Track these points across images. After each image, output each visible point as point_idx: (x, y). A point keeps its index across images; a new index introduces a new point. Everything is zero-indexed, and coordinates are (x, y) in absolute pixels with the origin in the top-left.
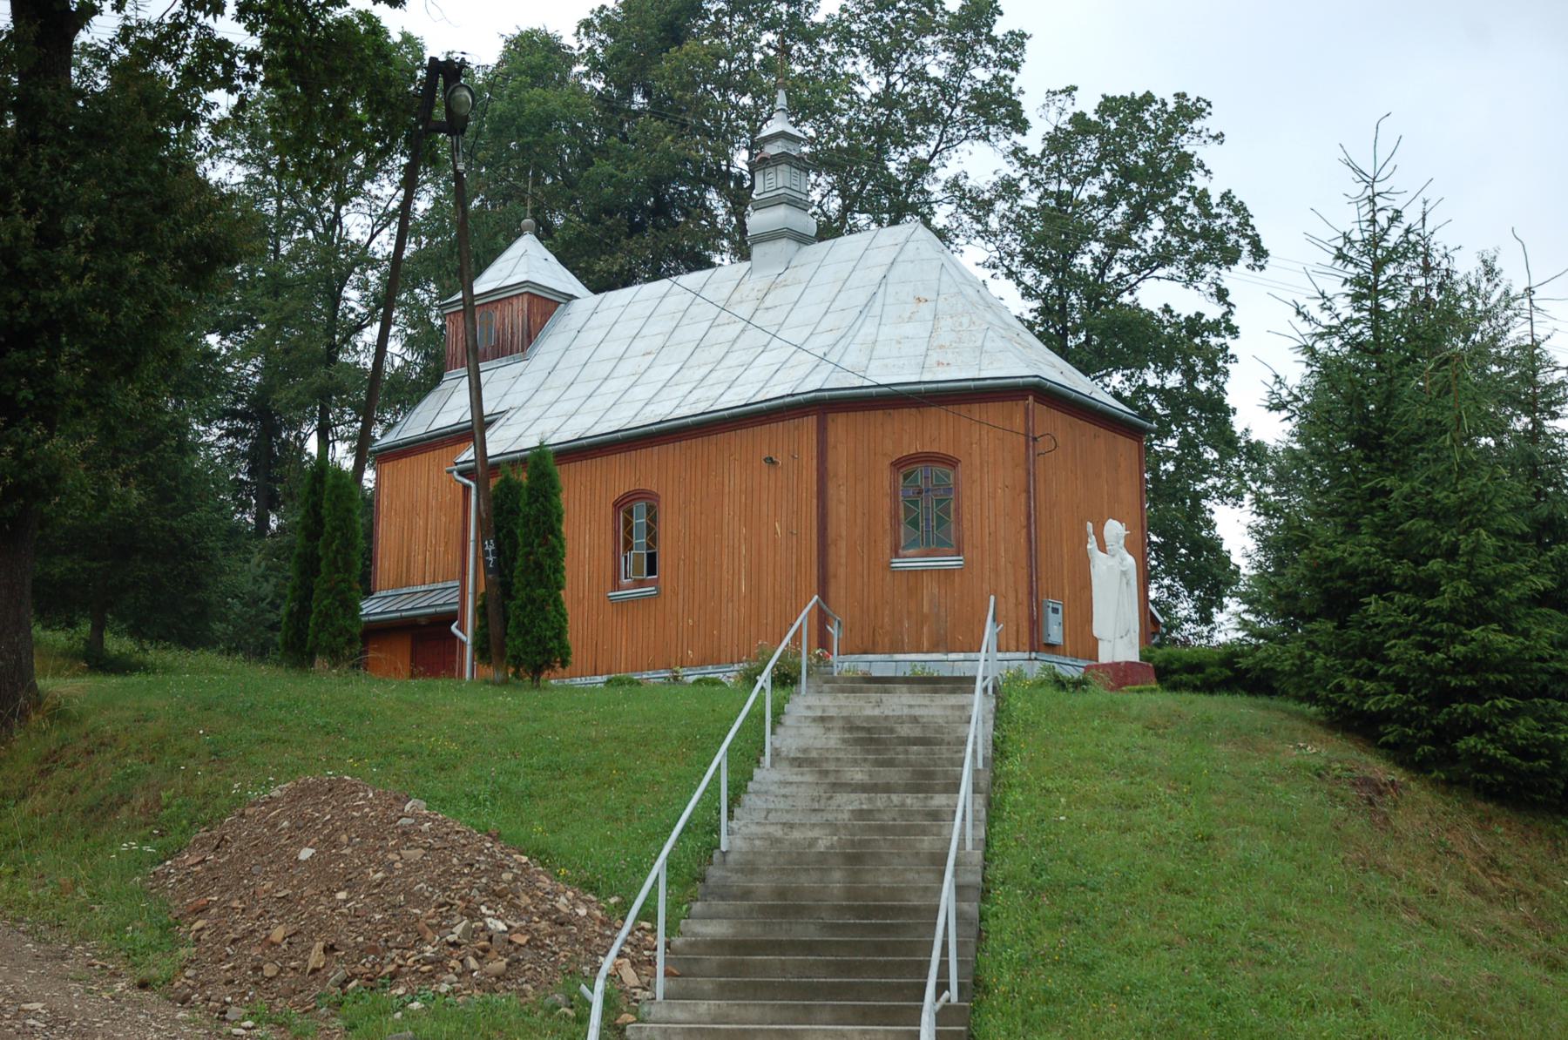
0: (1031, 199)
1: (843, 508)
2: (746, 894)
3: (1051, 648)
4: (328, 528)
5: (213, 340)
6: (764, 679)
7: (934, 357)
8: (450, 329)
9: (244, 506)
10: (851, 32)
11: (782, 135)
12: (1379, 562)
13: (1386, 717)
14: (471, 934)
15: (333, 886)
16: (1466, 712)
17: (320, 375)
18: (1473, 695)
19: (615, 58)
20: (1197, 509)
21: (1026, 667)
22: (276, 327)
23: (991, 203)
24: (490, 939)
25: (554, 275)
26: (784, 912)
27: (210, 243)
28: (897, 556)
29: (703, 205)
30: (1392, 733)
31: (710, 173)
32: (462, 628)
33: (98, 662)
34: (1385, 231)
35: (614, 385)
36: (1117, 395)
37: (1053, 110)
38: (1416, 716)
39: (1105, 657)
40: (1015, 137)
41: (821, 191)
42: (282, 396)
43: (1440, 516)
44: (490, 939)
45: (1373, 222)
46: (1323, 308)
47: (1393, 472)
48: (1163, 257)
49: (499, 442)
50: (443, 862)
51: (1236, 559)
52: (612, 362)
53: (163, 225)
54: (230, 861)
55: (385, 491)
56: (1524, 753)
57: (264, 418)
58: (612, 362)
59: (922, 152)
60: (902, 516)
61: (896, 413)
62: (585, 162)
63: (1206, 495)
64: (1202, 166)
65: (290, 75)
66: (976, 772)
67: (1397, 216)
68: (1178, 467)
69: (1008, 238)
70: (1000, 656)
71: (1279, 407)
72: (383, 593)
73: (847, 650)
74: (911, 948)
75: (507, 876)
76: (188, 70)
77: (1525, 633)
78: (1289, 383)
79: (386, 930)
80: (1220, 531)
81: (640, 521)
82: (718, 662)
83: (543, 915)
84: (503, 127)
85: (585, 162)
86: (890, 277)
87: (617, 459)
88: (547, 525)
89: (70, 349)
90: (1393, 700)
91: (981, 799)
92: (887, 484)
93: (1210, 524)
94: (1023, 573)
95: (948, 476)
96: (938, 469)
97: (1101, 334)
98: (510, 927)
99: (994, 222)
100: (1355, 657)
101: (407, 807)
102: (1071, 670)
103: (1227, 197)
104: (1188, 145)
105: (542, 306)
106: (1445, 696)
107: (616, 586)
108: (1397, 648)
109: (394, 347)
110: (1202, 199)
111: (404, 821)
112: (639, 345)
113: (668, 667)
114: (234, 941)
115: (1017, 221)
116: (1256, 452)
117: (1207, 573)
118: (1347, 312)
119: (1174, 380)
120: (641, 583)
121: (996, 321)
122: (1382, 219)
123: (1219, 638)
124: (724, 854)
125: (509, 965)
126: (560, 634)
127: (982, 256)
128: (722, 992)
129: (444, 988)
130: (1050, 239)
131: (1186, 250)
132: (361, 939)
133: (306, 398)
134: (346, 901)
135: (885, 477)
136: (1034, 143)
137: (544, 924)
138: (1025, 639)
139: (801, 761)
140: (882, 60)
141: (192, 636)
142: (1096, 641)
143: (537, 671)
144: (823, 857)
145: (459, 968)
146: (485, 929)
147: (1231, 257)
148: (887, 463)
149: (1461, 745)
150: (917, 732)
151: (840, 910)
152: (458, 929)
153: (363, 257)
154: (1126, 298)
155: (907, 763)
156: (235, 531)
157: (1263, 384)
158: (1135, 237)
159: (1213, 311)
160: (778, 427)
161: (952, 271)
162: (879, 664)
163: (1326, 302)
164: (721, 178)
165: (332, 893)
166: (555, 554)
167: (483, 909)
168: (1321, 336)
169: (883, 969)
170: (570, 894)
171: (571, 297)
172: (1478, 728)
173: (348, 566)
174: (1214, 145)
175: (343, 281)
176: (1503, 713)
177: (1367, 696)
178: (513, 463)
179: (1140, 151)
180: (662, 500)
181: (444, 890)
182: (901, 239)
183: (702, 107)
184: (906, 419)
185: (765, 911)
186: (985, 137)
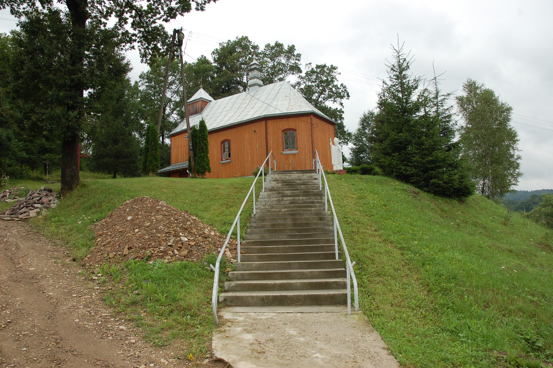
2: (263, 227)
7: (290, 108)
11: (255, 64)
13: (412, 175)
14: (176, 242)
15: (135, 228)
16: (432, 174)
18: (432, 169)
19: (219, 58)
24: (182, 244)
26: (275, 231)
30: (414, 179)
35: (220, 118)
37: (307, 68)
38: (419, 175)
44: (182, 244)
45: (400, 62)
48: (330, 97)
50: (168, 219)
52: (220, 113)
54: (112, 221)
55: (173, 146)
56: (445, 183)
58: (220, 113)
61: (283, 120)
67: (405, 60)
74: (328, 241)
75: (189, 223)
79: (149, 241)
81: (227, 146)
83: (200, 235)
87: (221, 133)
90: (414, 171)
96: (292, 132)
98: (189, 239)
103: (342, 85)
105: (205, 103)
106: (426, 171)
107: (222, 160)
110: (336, 86)
111: (158, 207)
112: (225, 109)
114: (104, 245)
120: (227, 159)
122: (401, 61)
124: (255, 215)
125: (188, 252)
126: (208, 165)
128: (260, 258)
129: (166, 261)
132: (140, 245)
134: (138, 232)
135: (280, 134)
136: (303, 75)
139: (272, 190)
140: (272, 59)
146: (181, 240)
147: (342, 97)
149: (432, 181)
150: (302, 181)
151: (292, 230)
152: (172, 241)
153: (170, 100)
155: (301, 189)
159: (339, 107)
165: (134, 229)
167: (181, 234)
169: (311, 249)
170: (209, 228)
172: (435, 177)
174: (339, 75)
177: (408, 171)
181: (168, 228)
185: (269, 231)
186: (293, 74)
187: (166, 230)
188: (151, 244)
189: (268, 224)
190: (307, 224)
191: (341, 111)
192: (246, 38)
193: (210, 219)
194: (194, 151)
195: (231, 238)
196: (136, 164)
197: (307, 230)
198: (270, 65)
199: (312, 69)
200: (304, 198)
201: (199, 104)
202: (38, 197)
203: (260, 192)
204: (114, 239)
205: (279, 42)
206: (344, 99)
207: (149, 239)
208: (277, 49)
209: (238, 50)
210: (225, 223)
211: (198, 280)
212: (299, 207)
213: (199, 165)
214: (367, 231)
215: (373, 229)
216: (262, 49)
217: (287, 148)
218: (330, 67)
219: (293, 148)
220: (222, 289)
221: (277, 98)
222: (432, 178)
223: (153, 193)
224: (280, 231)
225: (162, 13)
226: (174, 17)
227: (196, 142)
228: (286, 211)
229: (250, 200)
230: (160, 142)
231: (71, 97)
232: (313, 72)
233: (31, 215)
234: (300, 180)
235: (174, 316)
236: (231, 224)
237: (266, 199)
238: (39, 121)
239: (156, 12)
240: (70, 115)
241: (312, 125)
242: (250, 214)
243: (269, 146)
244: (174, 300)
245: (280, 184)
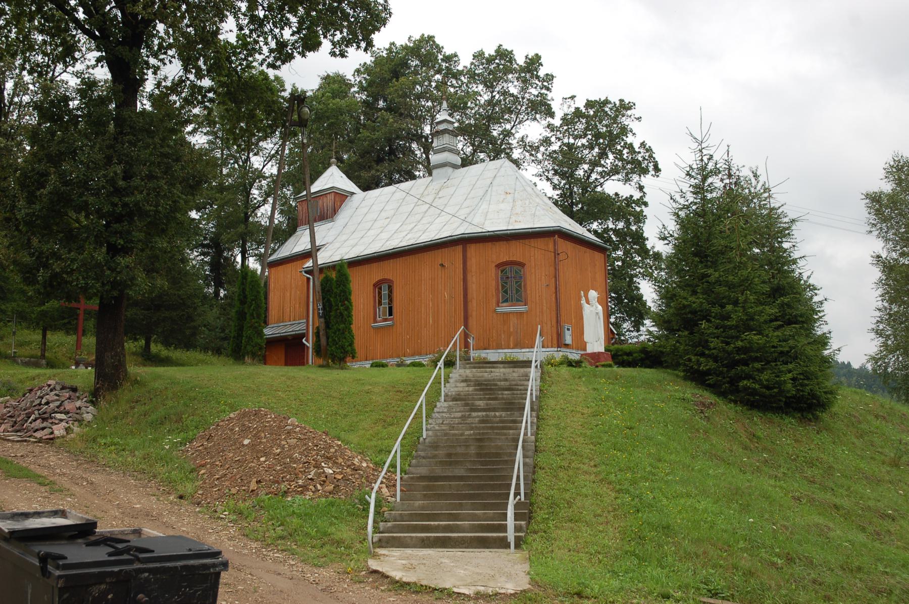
0: (555, 147)
1: (474, 286)
2: (434, 457)
3: (567, 346)
4: (249, 300)
5: (194, 215)
6: (441, 364)
7: (513, 218)
8: (300, 208)
9: (208, 285)
10: (475, 74)
12: (706, 306)
13: (708, 373)
15: (259, 455)
17: (241, 228)
20: (631, 282)
21: (556, 354)
22: (221, 207)
23: (538, 147)
25: (344, 183)
26: (450, 463)
27: (194, 175)
29: (410, 150)
30: (712, 379)
31: (414, 135)
32: (307, 340)
33: (149, 358)
34: (707, 164)
35: (371, 232)
36: (595, 232)
37: (566, 106)
38: (721, 373)
39: (590, 349)
40: (549, 119)
41: (461, 144)
42: (224, 237)
43: (731, 286)
45: (702, 160)
46: (682, 197)
47: (711, 267)
48: (615, 171)
49: (324, 258)
51: (649, 303)
52: (369, 222)
53: (177, 167)
54: (214, 445)
56: (768, 388)
57: (216, 247)
58: (369, 222)
59: (508, 127)
61: (497, 244)
62: (357, 130)
63: (636, 276)
64: (631, 131)
65: (230, 99)
66: (532, 402)
68: (623, 263)
69: (546, 163)
70: (544, 350)
71: (664, 238)
73: (477, 348)
75: (332, 450)
76: (185, 99)
77: (767, 336)
78: (669, 229)
80: (642, 291)
81: (385, 292)
82: (420, 354)
83: (348, 466)
84: (320, 117)
85: (357, 130)
87: (374, 266)
88: (345, 296)
89: (139, 223)
90: (712, 365)
91: (534, 414)
92: (493, 275)
93: (638, 289)
94: (554, 313)
96: (515, 267)
97: (589, 205)
99: (540, 156)
100: (697, 347)
101: (289, 421)
102: (574, 356)
103: (643, 144)
104: (625, 121)
105: (341, 197)
106: (734, 364)
108: (714, 343)
109: (277, 215)
110: (630, 147)
112: (384, 214)
113: (398, 357)
115: (550, 155)
116: (657, 256)
117: (635, 310)
118: (691, 200)
119: (621, 225)
120: (385, 320)
121: (541, 202)
122: (705, 159)
123: (642, 338)
126: (351, 344)
127: (535, 171)
128: (425, 497)
129: (308, 497)
130: (565, 163)
131: (624, 168)
133: (235, 238)
135: (493, 272)
136: (557, 122)
137: (348, 470)
138: (555, 342)
140: (490, 86)
141: (188, 345)
142: (586, 343)
143: (342, 360)
144: (466, 440)
145: (313, 489)
146: (324, 472)
147: (645, 171)
148: (494, 265)
150: (507, 383)
152: (312, 473)
153: (260, 175)
154: (599, 189)
155: (503, 399)
156: (205, 297)
157: (659, 229)
158: (602, 162)
159: (637, 195)
160: (445, 251)
161: (522, 181)
162: (493, 355)
163: (683, 194)
164: (419, 137)
166: (348, 309)
168: (681, 209)
169: (493, 487)
171: (353, 193)
172: (748, 377)
173: (259, 316)
175: (251, 186)
176: (758, 370)
178: (329, 267)
179: (603, 124)
182: (498, 166)
183: (409, 107)
184: (501, 247)
186: (535, 119)
187: (304, 459)
188: (285, 477)
189: (441, 452)
190: (498, 455)
191: (642, 202)
192: (431, 38)
193: (359, 444)
194: (325, 319)
195: (388, 471)
196: (193, 321)
197: (494, 463)
198: (486, 97)
199: (577, 109)
200: (503, 414)
201: (329, 201)
202: (57, 400)
203: (435, 400)
204: (230, 470)
205: (504, 47)
206: (649, 176)
207: (280, 470)
208: (497, 65)
209: (414, 63)
210: (381, 451)
211: (349, 519)
212: (492, 428)
213: (336, 346)
214: (582, 466)
215: (592, 463)
216: (465, 61)
217: (506, 301)
218: (618, 103)
219: (518, 300)
220: (376, 530)
221: (488, 197)
222: (741, 378)
223: (263, 398)
224: (457, 463)
225: (265, 50)
226: (289, 58)
227: (329, 300)
228: (471, 435)
229: (418, 416)
230: (239, 266)
231: (120, 233)
232: (578, 113)
233: (57, 433)
234: (506, 380)
235: (328, 547)
236: (390, 452)
237: (444, 415)
238: (67, 273)
239: (254, 49)
240: (119, 264)
241: (556, 254)
242: (418, 438)
243: (469, 296)
244: (326, 534)
245: (471, 389)
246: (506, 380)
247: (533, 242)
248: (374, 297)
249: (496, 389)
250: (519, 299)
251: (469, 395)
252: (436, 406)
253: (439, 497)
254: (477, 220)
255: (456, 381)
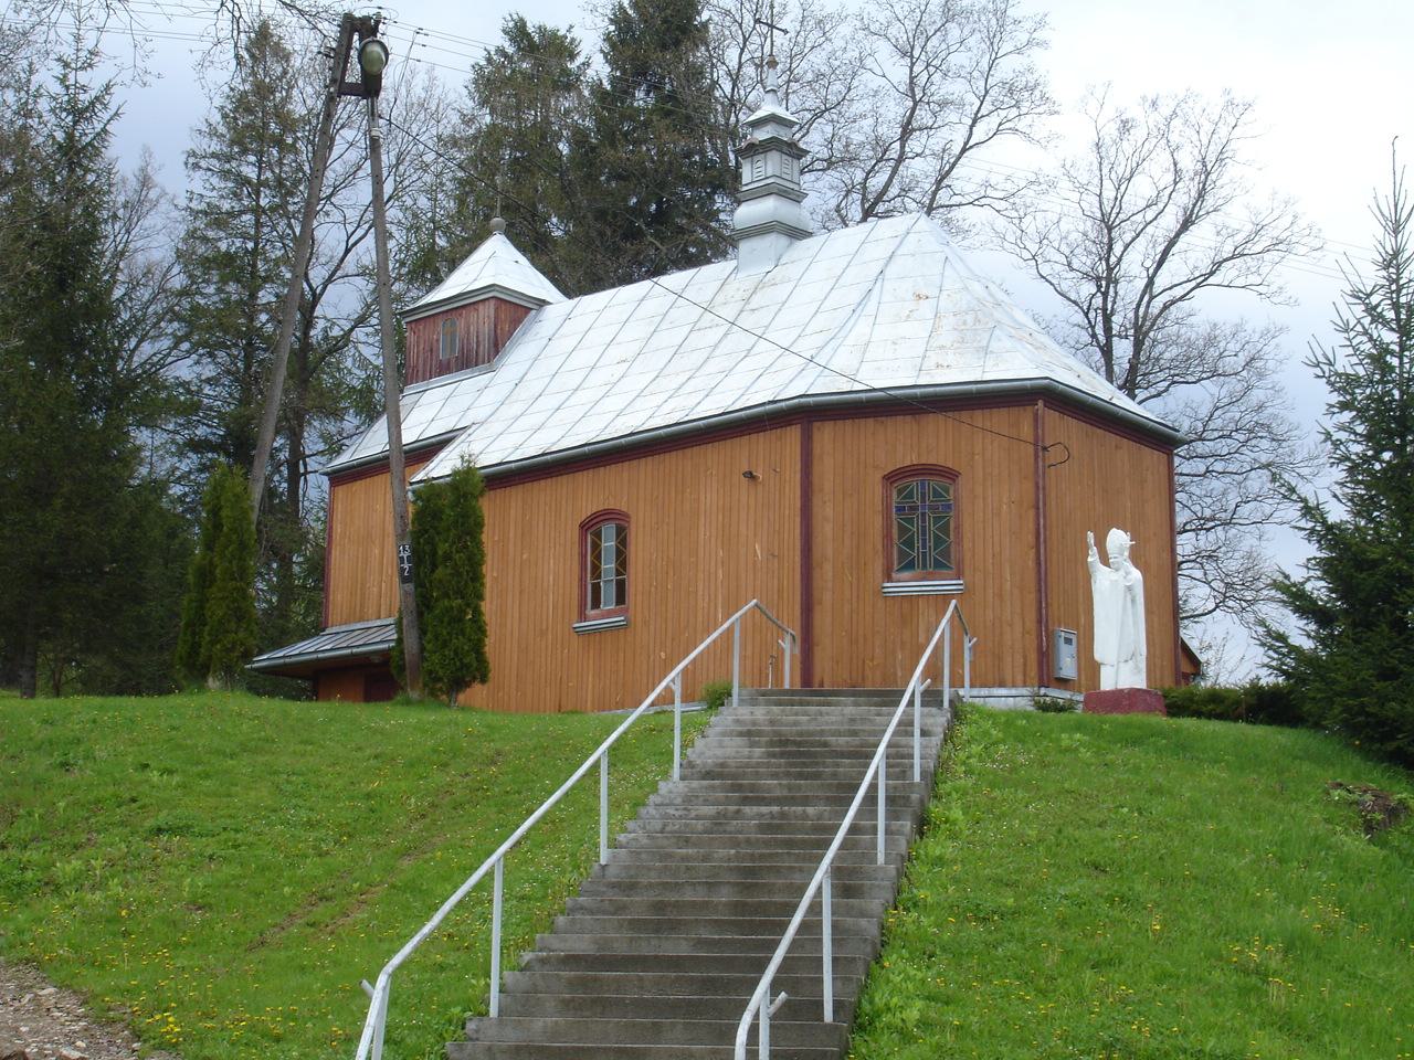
2: (620, 908)
7: (933, 358)
26: (658, 928)
28: (890, 579)
52: (594, 366)
60: (895, 536)
61: (890, 421)
72: (334, 630)
81: (609, 543)
86: (888, 272)
87: (584, 478)
94: (1031, 597)
95: (947, 492)
96: (934, 482)
105: (513, 312)
112: (615, 353)
124: (604, 867)
135: (875, 490)
138: (1033, 673)
148: (879, 476)
150: (856, 740)
171: (542, 303)
180: (633, 520)
182: (902, 229)
217: (910, 566)
219: (938, 565)
221: (871, 306)
224: (674, 926)
234: (854, 733)
245: (758, 751)
246: (854, 733)
247: (980, 417)
248: (583, 556)
249: (823, 755)
250: (941, 560)
251: (747, 765)
252: (655, 790)
253: (603, 1006)
254: (843, 360)
255: (724, 734)
